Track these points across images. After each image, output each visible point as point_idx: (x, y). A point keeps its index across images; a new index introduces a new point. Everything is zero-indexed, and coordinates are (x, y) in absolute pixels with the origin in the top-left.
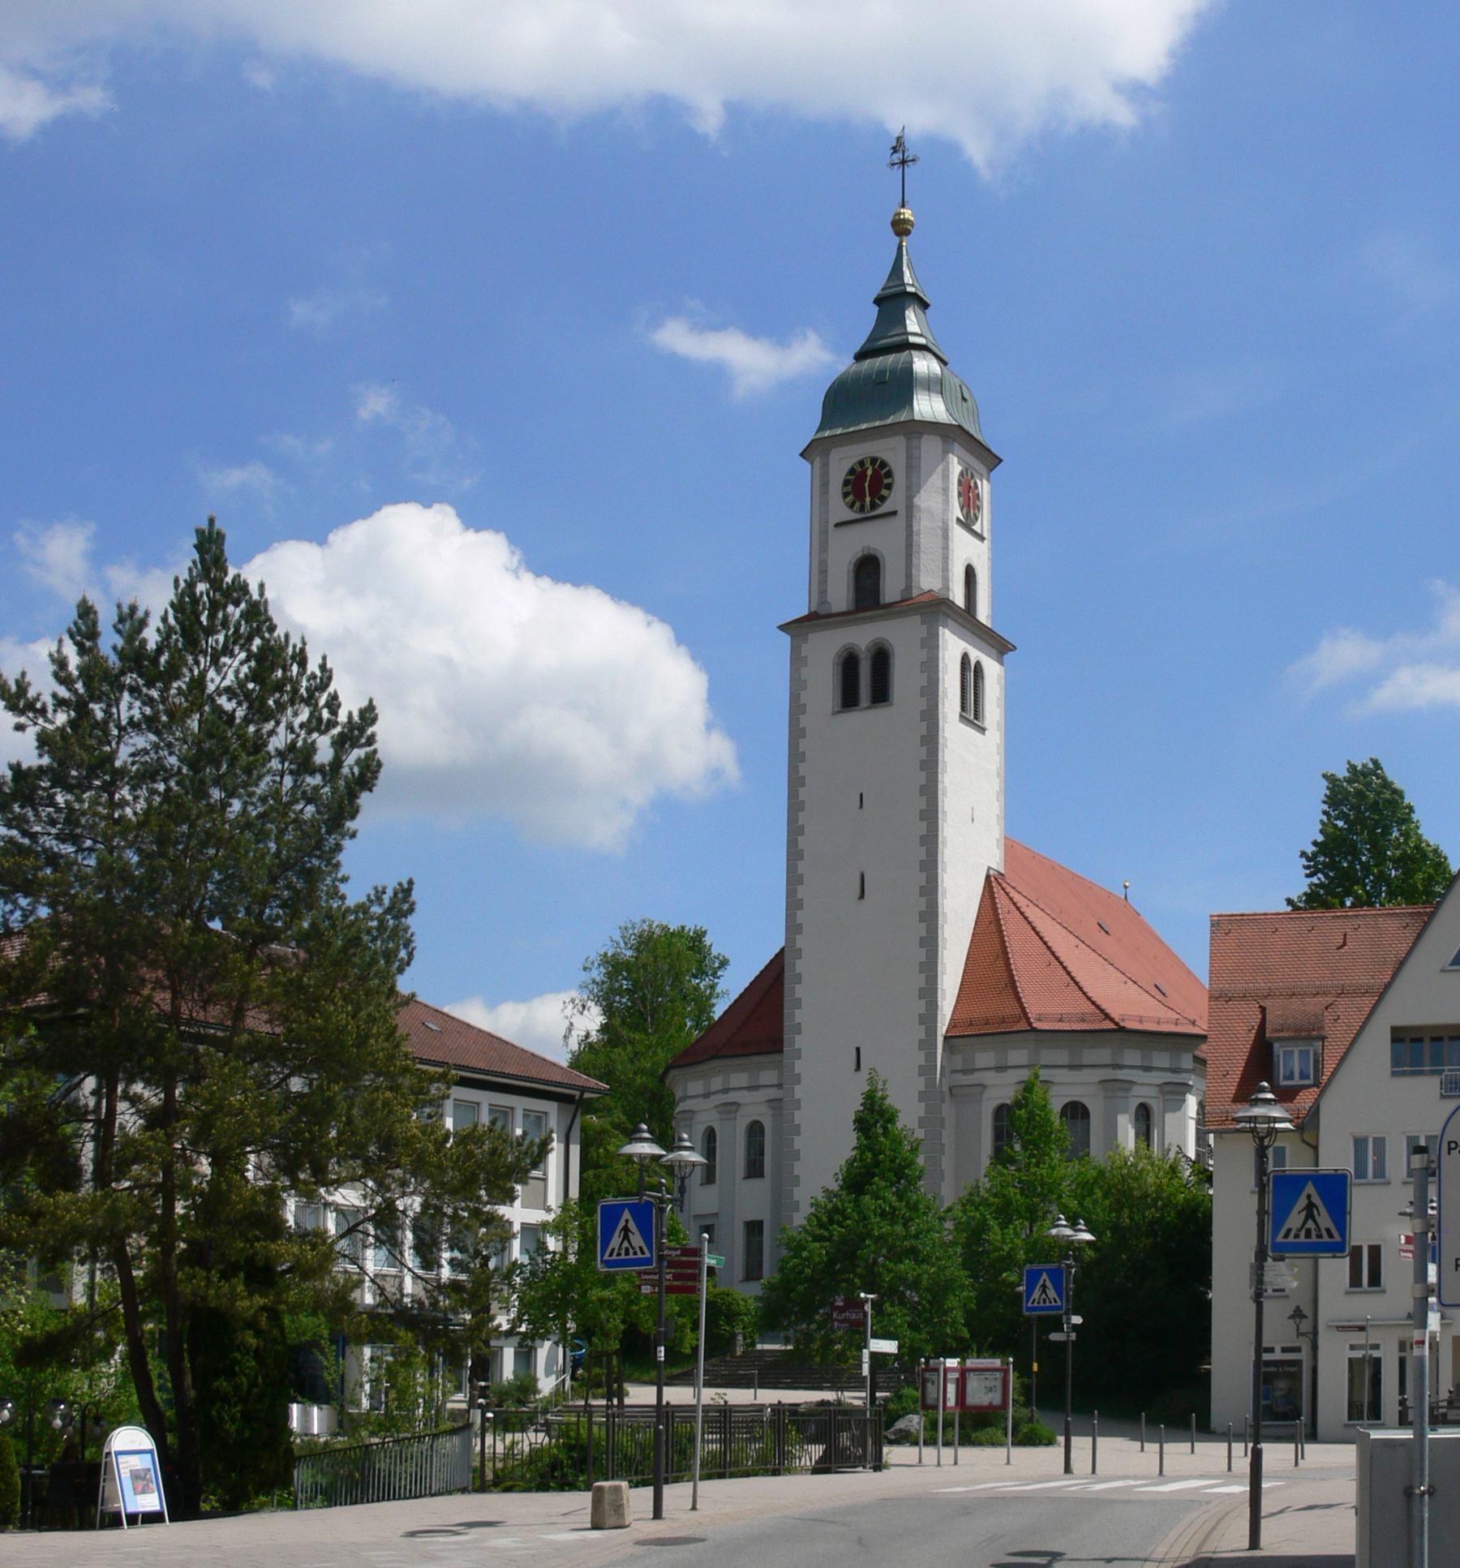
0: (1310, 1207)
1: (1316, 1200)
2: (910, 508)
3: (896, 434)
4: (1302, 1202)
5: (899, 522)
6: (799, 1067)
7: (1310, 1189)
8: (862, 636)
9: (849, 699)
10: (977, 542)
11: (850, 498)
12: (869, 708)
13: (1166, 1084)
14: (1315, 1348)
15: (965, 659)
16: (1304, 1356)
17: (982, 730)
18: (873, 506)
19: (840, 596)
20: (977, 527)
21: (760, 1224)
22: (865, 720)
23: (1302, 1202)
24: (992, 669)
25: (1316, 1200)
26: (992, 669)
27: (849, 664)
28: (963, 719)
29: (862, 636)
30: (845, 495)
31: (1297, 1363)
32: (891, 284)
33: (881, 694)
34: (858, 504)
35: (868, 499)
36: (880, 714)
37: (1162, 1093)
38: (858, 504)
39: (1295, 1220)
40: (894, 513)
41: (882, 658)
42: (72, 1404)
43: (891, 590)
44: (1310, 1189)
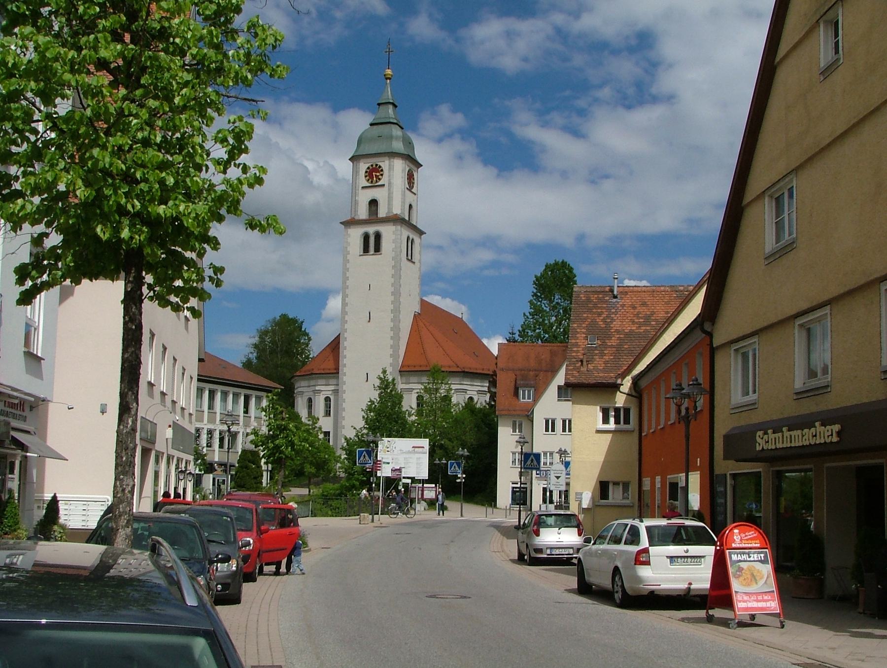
0: (532, 460)
1: (533, 458)
2: (390, 184)
3: (385, 156)
4: (531, 459)
5: (386, 188)
6: (345, 378)
7: (532, 456)
8: (371, 230)
9: (366, 250)
10: (413, 195)
11: (368, 178)
12: (373, 255)
13: (479, 391)
14: (531, 483)
15: (408, 238)
16: (528, 486)
17: (414, 263)
18: (376, 182)
19: (363, 213)
20: (413, 190)
21: (329, 432)
22: (371, 259)
23: (531, 459)
24: (417, 240)
25: (533, 458)
26: (417, 240)
27: (366, 237)
28: (408, 259)
29: (371, 230)
30: (366, 176)
31: (526, 488)
32: (371, 218)
33: (377, 249)
34: (370, 180)
35: (375, 179)
36: (377, 257)
37: (478, 394)
38: (370, 180)
39: (529, 462)
40: (384, 185)
41: (378, 236)
42: (242, 46)
43: (382, 212)
44: (532, 456)
